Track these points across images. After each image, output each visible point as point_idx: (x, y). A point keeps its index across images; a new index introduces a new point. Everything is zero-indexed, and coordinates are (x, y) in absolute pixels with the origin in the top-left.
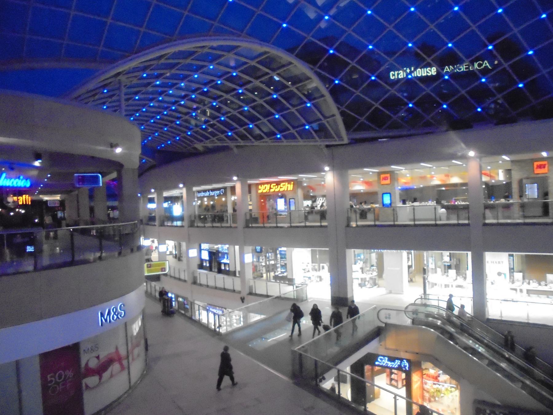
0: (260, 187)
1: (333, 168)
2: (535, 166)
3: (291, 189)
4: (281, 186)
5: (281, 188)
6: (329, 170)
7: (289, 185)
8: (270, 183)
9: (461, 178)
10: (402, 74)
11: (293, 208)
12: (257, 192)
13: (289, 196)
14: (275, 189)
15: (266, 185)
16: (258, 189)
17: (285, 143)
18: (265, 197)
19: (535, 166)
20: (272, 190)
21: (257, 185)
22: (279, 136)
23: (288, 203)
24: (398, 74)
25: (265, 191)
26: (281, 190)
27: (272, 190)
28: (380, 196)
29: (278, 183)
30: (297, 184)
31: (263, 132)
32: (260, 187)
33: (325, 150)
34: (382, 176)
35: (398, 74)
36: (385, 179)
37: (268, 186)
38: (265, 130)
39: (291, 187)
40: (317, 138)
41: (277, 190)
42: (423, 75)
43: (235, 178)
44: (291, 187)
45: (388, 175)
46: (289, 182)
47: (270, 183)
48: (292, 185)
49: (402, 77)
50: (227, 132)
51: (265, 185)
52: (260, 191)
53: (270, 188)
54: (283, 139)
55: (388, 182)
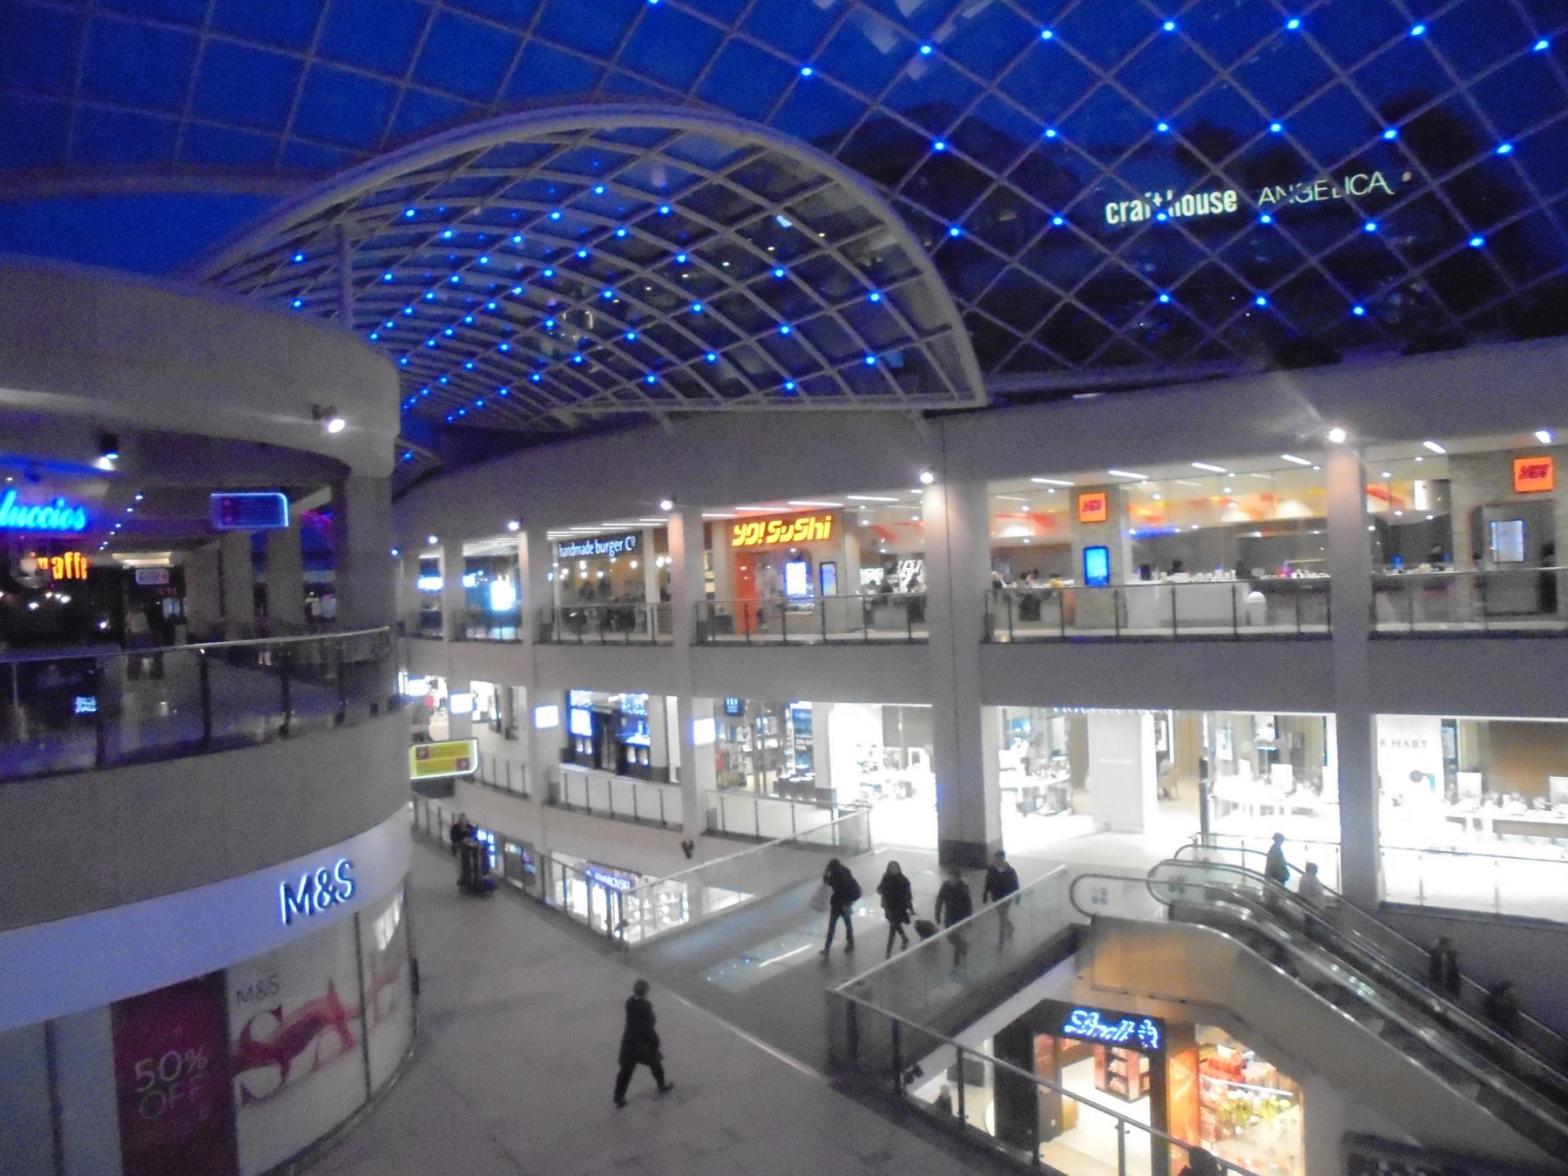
0: (736, 530)
1: (945, 475)
2: (1518, 471)
3: (826, 536)
4: (798, 527)
5: (796, 532)
6: (934, 483)
7: (820, 525)
8: (766, 519)
9: (1308, 503)
10: (1139, 209)
11: (830, 589)
12: (729, 543)
13: (819, 555)
14: (780, 535)
15: (754, 525)
16: (730, 536)
17: (808, 404)
18: (752, 557)
19: (1518, 471)
20: (770, 539)
21: (730, 523)
22: (790, 386)
23: (815, 576)
24: (1129, 210)
25: (750, 541)
26: (798, 537)
27: (770, 539)
28: (1077, 555)
29: (788, 520)
30: (843, 521)
31: (745, 373)
32: (736, 530)
33: (923, 426)
34: (1085, 499)
35: (1129, 210)
36: (1092, 506)
37: (759, 528)
38: (752, 368)
39: (824, 530)
40: (899, 392)
41: (785, 538)
42: (1200, 212)
43: (666, 505)
44: (824, 530)
45: (1101, 497)
46: (819, 514)
47: (766, 519)
48: (828, 525)
49: (1140, 217)
50: (644, 375)
51: (752, 526)
52: (736, 543)
53: (767, 533)
54: (803, 395)
55: (1100, 515)
